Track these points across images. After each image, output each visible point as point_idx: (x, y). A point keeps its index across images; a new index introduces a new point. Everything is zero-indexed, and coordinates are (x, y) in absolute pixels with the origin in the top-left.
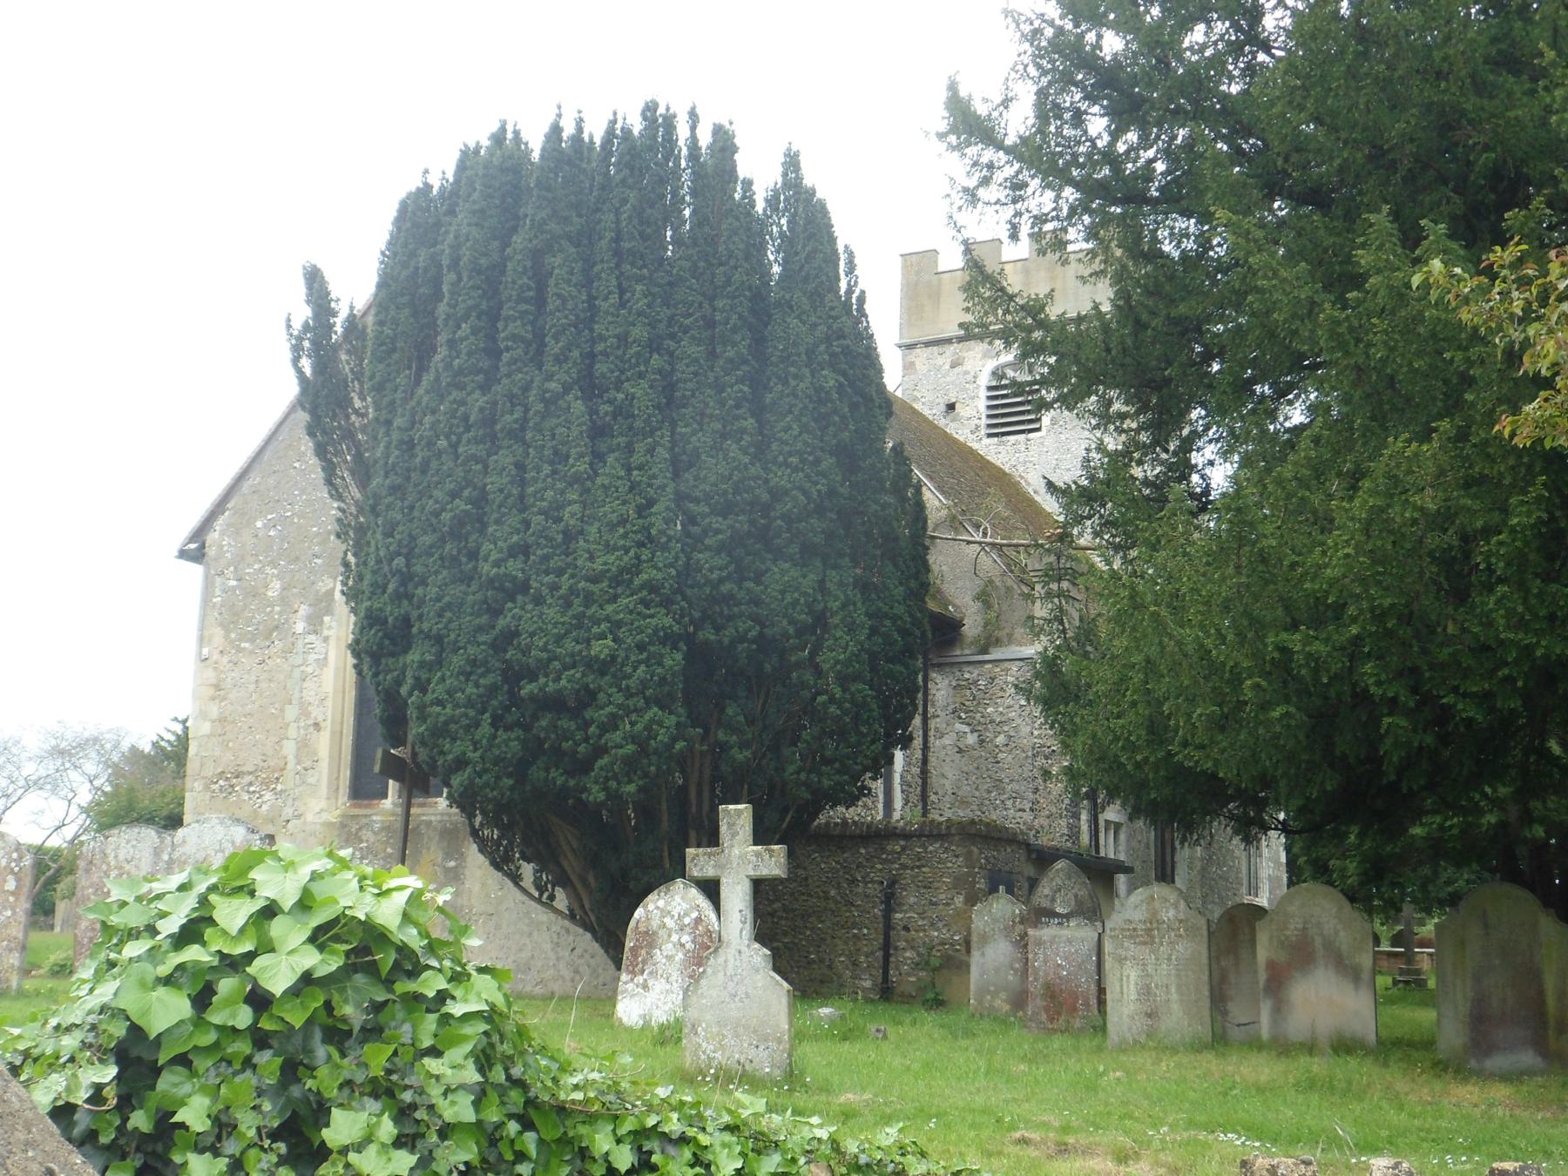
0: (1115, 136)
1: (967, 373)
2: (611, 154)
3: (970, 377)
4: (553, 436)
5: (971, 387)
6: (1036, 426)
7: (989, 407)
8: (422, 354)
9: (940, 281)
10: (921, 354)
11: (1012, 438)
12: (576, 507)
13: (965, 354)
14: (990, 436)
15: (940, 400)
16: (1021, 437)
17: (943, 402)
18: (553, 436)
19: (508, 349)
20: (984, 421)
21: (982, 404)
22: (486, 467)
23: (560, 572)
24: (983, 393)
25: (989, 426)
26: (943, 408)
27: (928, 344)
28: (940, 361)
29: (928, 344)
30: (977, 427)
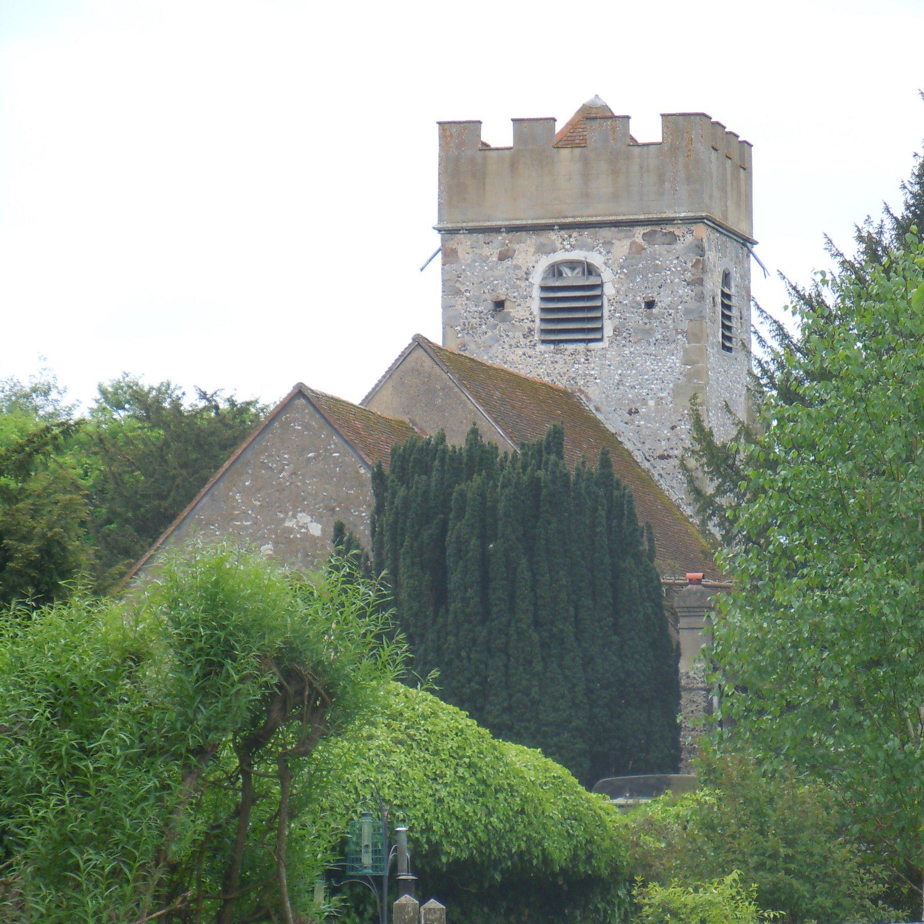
0: (787, 453)
1: (517, 267)
2: (517, 460)
3: (521, 273)
4: (523, 651)
5: (523, 284)
6: (598, 336)
7: (544, 310)
8: (441, 596)
9: (485, 158)
10: (463, 244)
11: (571, 347)
12: (537, 689)
13: (516, 246)
14: (543, 342)
15: (487, 296)
16: (581, 347)
17: (490, 298)
18: (523, 651)
19: (496, 605)
20: (538, 325)
21: (535, 305)
22: (487, 666)
23: (529, 721)
24: (536, 293)
25: (544, 331)
26: (491, 306)
27: (472, 231)
28: (486, 251)
29: (472, 231)
30: (531, 330)
